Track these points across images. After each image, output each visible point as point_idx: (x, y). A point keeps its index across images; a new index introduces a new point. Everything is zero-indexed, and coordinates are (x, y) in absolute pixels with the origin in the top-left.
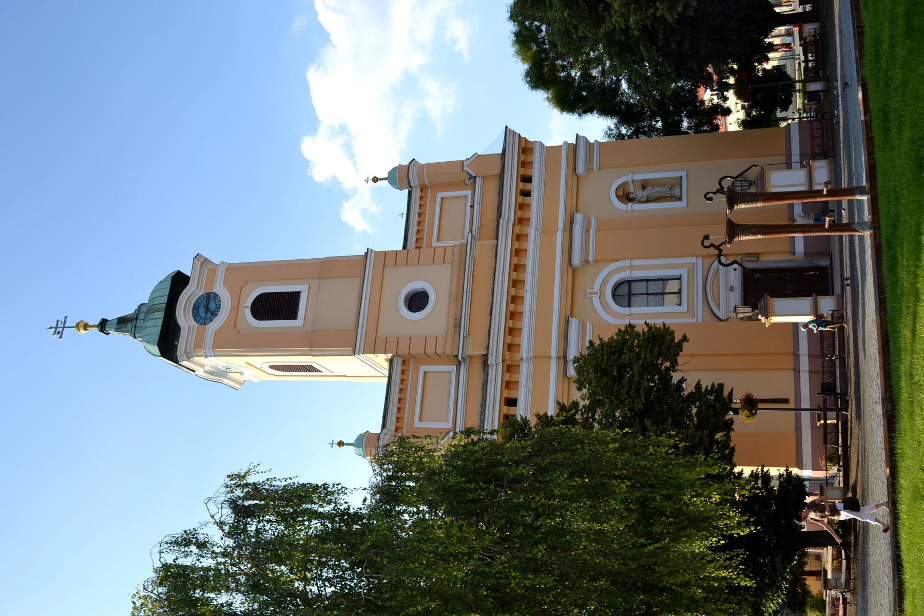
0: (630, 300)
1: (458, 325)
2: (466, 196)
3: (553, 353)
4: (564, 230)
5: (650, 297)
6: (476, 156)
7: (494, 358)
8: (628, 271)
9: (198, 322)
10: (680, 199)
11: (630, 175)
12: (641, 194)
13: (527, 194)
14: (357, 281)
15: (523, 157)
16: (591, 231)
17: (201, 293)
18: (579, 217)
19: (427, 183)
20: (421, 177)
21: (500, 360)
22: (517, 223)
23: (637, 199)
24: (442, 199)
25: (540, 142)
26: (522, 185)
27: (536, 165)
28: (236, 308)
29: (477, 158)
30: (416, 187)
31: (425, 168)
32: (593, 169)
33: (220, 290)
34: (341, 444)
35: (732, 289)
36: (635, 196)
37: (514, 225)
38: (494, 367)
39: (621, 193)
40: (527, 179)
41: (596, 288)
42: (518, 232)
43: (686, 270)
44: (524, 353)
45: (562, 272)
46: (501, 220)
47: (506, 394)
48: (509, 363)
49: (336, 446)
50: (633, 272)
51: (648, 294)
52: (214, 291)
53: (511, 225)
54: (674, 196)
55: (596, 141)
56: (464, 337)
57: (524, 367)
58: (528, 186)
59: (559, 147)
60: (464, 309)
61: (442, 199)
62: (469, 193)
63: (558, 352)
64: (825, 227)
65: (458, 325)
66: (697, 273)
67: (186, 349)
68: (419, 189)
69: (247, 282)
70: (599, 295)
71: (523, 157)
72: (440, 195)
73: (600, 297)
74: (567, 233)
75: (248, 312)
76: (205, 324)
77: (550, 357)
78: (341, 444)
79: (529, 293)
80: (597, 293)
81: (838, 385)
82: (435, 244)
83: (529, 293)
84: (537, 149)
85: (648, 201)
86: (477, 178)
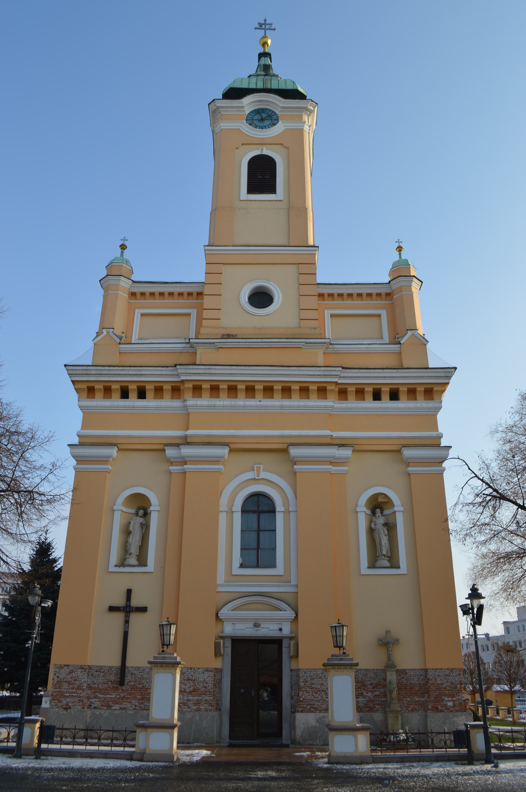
0: (253, 512)
1: (229, 336)
2: (382, 338)
3: (190, 432)
4: (331, 437)
5: (254, 535)
6: (425, 342)
7: (183, 371)
8: (282, 509)
9: (249, 114)
10: (372, 565)
11: (402, 509)
12: (380, 520)
13: (125, 394)
14: (284, 242)
15: (420, 389)
16: (331, 467)
17: (278, 113)
18: (347, 452)
19: (403, 293)
20: (400, 289)
21: (183, 378)
22: (340, 387)
23: (374, 519)
24: (379, 316)
25: (440, 408)
26: (385, 390)
27: (412, 404)
28: (262, 143)
29: (423, 342)
30: (391, 287)
31: (409, 293)
32: (409, 467)
33: (279, 128)
34: (123, 247)
35: (256, 625)
36: (377, 516)
37: (336, 383)
38: (175, 373)
39: (380, 500)
40: (394, 396)
41: (263, 475)
42: (328, 388)
43: (152, 570)
44: (192, 402)
45: (283, 437)
46: (341, 369)
47: (149, 387)
48: (182, 388)
49: (397, 245)
50: (282, 514)
51: (259, 531)
52: (280, 122)
53: (335, 380)
54: (376, 561)
55: (444, 470)
56: (214, 343)
57: (176, 403)
58: (385, 396)
59: (436, 428)
60: (244, 340)
61: (379, 316)
62: (386, 339)
63: (192, 436)
64: (14, 747)
65: (229, 336)
66: (279, 586)
67: (222, 107)
68: (387, 291)
69: (288, 148)
70: (256, 478)
71: (420, 389)
72: (384, 313)
73: (255, 479)
74: (328, 441)
75: (257, 153)
76: (247, 120)
77: (187, 429)
78: (123, 247)
79: (258, 403)
80: (258, 475)
81: (51, 746)
82: (327, 313)
83: (258, 403)
84: (430, 404)
85: (371, 531)
86: (399, 346)
